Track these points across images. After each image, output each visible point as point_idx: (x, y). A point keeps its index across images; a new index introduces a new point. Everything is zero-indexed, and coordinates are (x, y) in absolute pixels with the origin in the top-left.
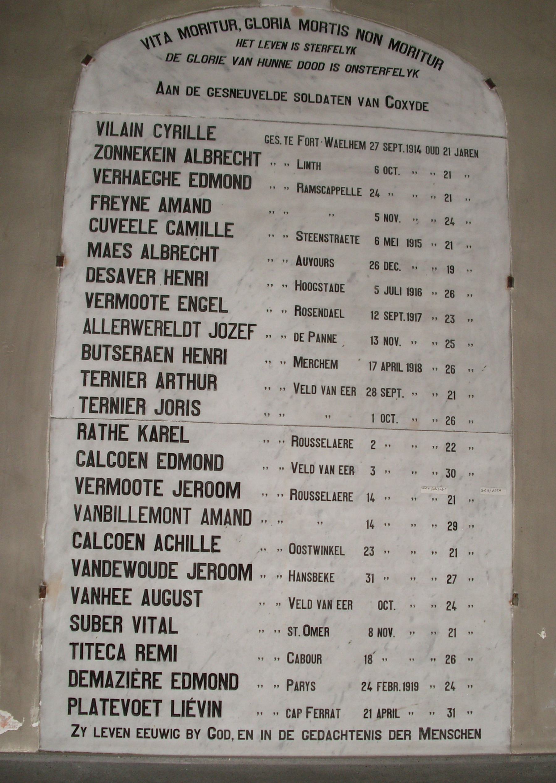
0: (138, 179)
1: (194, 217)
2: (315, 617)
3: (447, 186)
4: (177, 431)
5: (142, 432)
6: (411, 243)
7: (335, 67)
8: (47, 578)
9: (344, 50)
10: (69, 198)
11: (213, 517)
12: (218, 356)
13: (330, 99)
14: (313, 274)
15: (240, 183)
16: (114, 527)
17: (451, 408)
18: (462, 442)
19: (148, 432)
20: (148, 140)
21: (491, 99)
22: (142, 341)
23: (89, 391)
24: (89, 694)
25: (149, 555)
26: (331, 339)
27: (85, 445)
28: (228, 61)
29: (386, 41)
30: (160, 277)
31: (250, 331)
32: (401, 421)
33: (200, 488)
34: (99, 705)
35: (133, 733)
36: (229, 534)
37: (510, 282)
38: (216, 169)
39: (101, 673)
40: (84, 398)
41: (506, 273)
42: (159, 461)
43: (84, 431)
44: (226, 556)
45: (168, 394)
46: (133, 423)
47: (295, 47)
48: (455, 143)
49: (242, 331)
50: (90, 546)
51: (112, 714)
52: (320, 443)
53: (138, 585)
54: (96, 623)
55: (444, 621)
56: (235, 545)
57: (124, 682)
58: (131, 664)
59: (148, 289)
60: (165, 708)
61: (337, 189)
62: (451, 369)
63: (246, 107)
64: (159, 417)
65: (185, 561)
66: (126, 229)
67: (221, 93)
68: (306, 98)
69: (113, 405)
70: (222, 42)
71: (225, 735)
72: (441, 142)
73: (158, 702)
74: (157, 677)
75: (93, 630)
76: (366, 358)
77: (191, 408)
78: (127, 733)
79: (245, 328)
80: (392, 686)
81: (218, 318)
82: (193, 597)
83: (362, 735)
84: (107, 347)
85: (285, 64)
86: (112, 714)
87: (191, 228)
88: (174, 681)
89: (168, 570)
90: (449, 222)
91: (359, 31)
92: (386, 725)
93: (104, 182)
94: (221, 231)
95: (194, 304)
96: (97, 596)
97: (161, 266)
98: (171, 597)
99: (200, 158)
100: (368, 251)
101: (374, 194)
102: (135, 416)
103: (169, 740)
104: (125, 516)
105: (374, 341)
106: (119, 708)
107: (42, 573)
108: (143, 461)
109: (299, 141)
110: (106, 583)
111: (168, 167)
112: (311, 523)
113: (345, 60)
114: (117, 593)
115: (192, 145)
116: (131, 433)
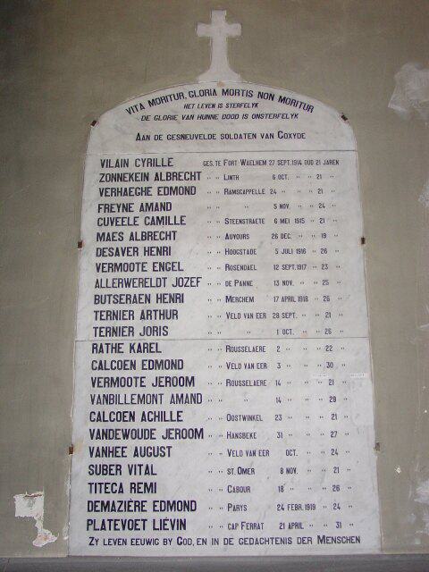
0: (126, 192)
1: (161, 214)
2: (245, 462)
3: (319, 184)
4: (154, 346)
5: (132, 347)
6: (297, 221)
7: (245, 116)
8: (73, 441)
9: (289, 116)
10: (85, 206)
11: (179, 399)
12: (178, 298)
13: (243, 137)
14: (237, 244)
15: (189, 191)
16: (116, 408)
17: (328, 323)
18: (336, 344)
19: (136, 347)
20: (132, 169)
21: (345, 128)
22: (131, 291)
23: (99, 324)
24: (99, 517)
25: (138, 424)
26: (249, 284)
27: (97, 357)
28: (179, 118)
29: (277, 98)
30: (141, 251)
31: (198, 282)
32: (296, 333)
33: (169, 381)
34: (107, 524)
35: (129, 542)
36: (188, 410)
37: (363, 240)
38: (174, 184)
39: (108, 502)
40: (96, 328)
41: (361, 235)
42: (143, 365)
43: (96, 348)
44: (187, 424)
45: (148, 323)
46: (126, 342)
47: (220, 106)
48: (324, 157)
49: (193, 282)
50: (100, 420)
51: (115, 529)
52: (244, 349)
53: (131, 444)
54: (105, 470)
55: (330, 462)
56: (192, 417)
57: (122, 508)
58: (127, 495)
59: (134, 259)
60: (149, 525)
61: (249, 191)
62: (327, 299)
63: (191, 145)
64: (142, 337)
65: (160, 428)
66: (120, 223)
67: (175, 137)
68: (227, 137)
69: (114, 331)
70: (176, 107)
71: (188, 542)
72: (314, 157)
73: (144, 520)
74: (144, 504)
75: (103, 474)
76: (272, 295)
77: (162, 331)
78: (125, 542)
79: (195, 280)
80: (298, 507)
81: (178, 274)
82: (166, 451)
83: (279, 541)
84: (110, 296)
85: (214, 117)
86: (115, 529)
87: (160, 220)
88: (155, 506)
89: (150, 434)
90: (322, 206)
91: (259, 93)
92: (295, 534)
93: (106, 195)
94: (178, 221)
95: (163, 267)
96: (106, 452)
97: (141, 245)
98: (152, 451)
99: (164, 177)
100: (270, 228)
101: (273, 192)
102: (128, 337)
103: (152, 546)
104: (122, 401)
105: (277, 283)
106: (119, 526)
107: (71, 438)
108: (133, 365)
109: (225, 163)
110: (111, 444)
111: (144, 184)
112: (240, 401)
113: (255, 111)
114: (118, 450)
115: (159, 170)
116: (125, 348)
